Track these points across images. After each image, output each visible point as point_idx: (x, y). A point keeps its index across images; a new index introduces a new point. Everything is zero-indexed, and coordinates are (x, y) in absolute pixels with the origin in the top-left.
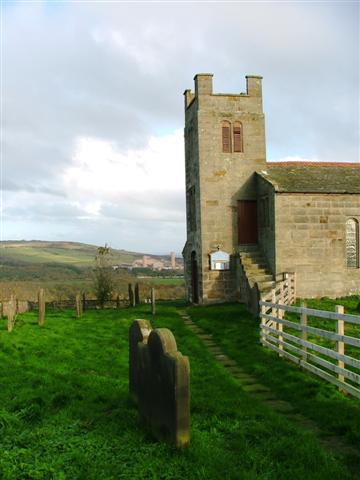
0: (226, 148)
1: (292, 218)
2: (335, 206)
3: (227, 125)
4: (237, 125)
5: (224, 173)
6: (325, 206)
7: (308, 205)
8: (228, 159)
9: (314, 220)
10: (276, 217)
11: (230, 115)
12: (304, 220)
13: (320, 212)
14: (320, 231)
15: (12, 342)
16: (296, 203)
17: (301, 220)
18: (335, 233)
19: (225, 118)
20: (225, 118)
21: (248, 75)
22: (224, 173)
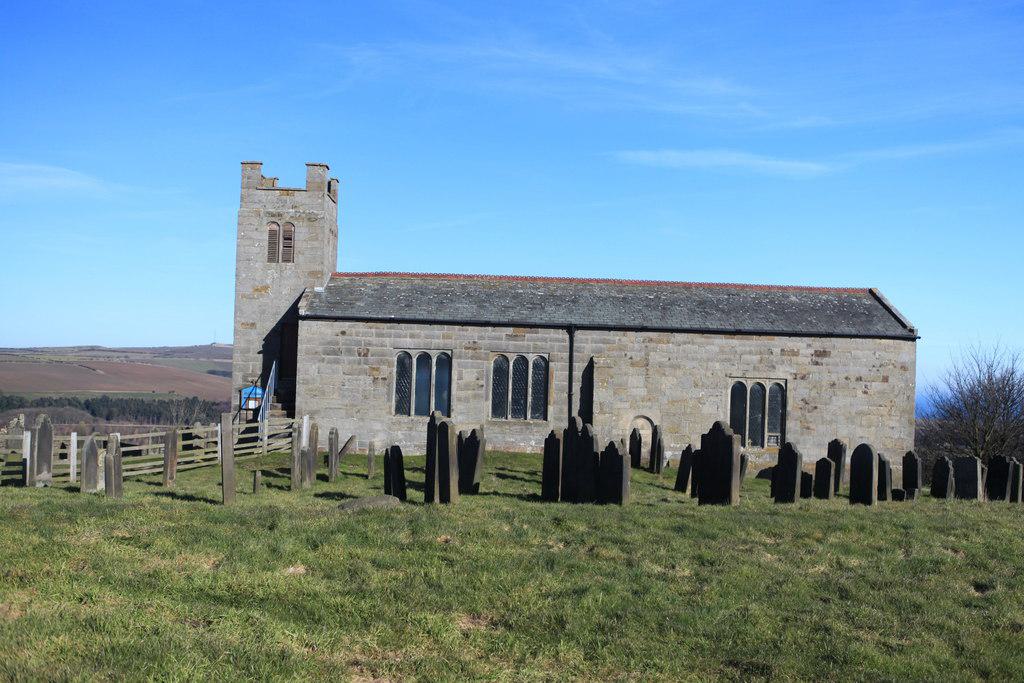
0: (272, 257)
1: (320, 349)
2: (379, 335)
3: (275, 227)
4: (288, 227)
5: (266, 288)
6: (365, 334)
7: (343, 333)
8: (273, 270)
9: (349, 352)
10: (299, 347)
11: (280, 215)
12: (335, 353)
13: (358, 343)
14: (355, 366)
15: (146, 622)
16: (329, 331)
17: (332, 351)
18: (377, 369)
19: (274, 219)
20: (274, 219)
21: (245, 161)
22: (266, 288)
